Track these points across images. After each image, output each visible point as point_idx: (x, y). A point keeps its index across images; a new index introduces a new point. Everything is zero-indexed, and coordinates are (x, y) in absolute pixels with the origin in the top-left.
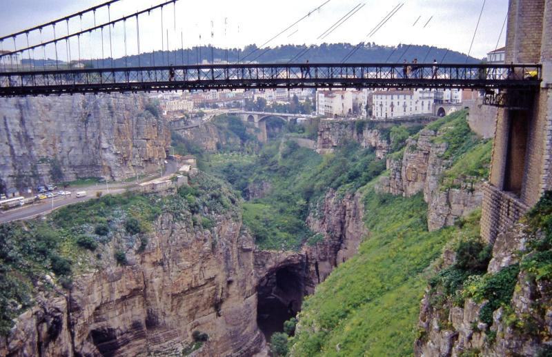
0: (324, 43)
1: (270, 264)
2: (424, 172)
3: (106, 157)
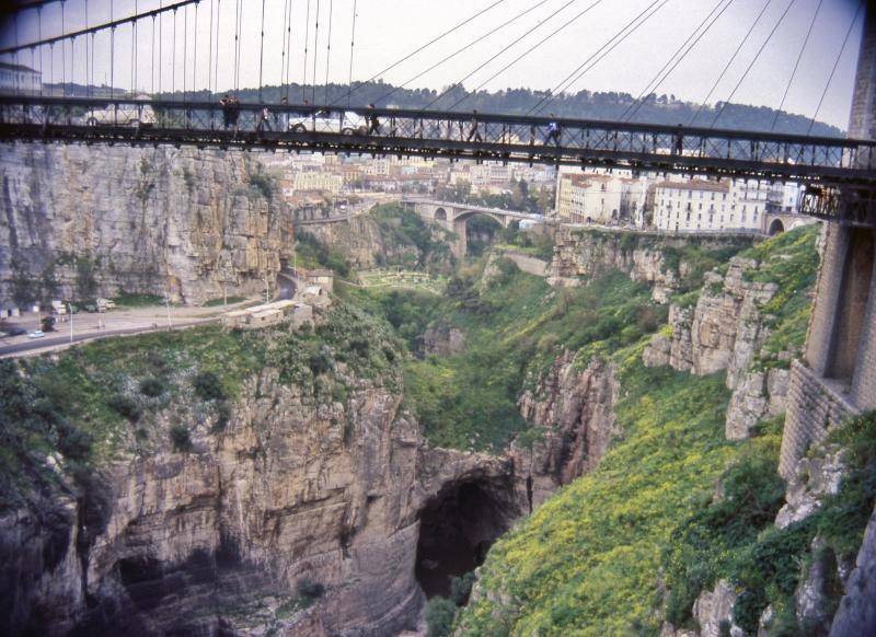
0: (584, 91)
1: (446, 473)
2: (731, 332)
3: (174, 262)
